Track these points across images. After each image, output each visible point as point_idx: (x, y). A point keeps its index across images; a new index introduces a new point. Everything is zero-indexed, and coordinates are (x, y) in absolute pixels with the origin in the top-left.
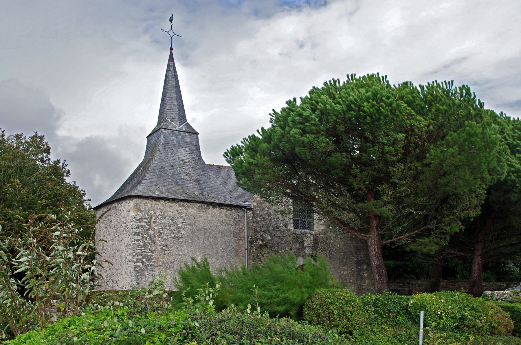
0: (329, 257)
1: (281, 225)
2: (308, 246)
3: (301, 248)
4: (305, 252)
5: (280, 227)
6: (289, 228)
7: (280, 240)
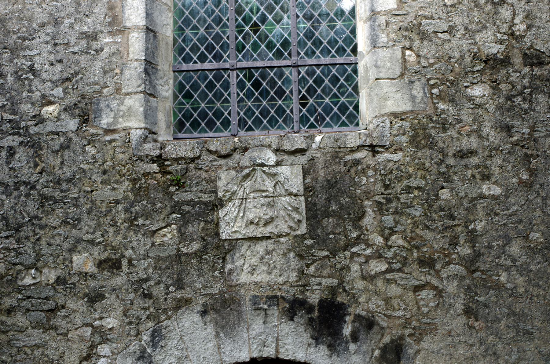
0: (468, 312)
1: (51, 110)
2: (251, 231)
3: (199, 255)
4: (226, 276)
5: (39, 120)
6: (105, 121)
7: (32, 207)
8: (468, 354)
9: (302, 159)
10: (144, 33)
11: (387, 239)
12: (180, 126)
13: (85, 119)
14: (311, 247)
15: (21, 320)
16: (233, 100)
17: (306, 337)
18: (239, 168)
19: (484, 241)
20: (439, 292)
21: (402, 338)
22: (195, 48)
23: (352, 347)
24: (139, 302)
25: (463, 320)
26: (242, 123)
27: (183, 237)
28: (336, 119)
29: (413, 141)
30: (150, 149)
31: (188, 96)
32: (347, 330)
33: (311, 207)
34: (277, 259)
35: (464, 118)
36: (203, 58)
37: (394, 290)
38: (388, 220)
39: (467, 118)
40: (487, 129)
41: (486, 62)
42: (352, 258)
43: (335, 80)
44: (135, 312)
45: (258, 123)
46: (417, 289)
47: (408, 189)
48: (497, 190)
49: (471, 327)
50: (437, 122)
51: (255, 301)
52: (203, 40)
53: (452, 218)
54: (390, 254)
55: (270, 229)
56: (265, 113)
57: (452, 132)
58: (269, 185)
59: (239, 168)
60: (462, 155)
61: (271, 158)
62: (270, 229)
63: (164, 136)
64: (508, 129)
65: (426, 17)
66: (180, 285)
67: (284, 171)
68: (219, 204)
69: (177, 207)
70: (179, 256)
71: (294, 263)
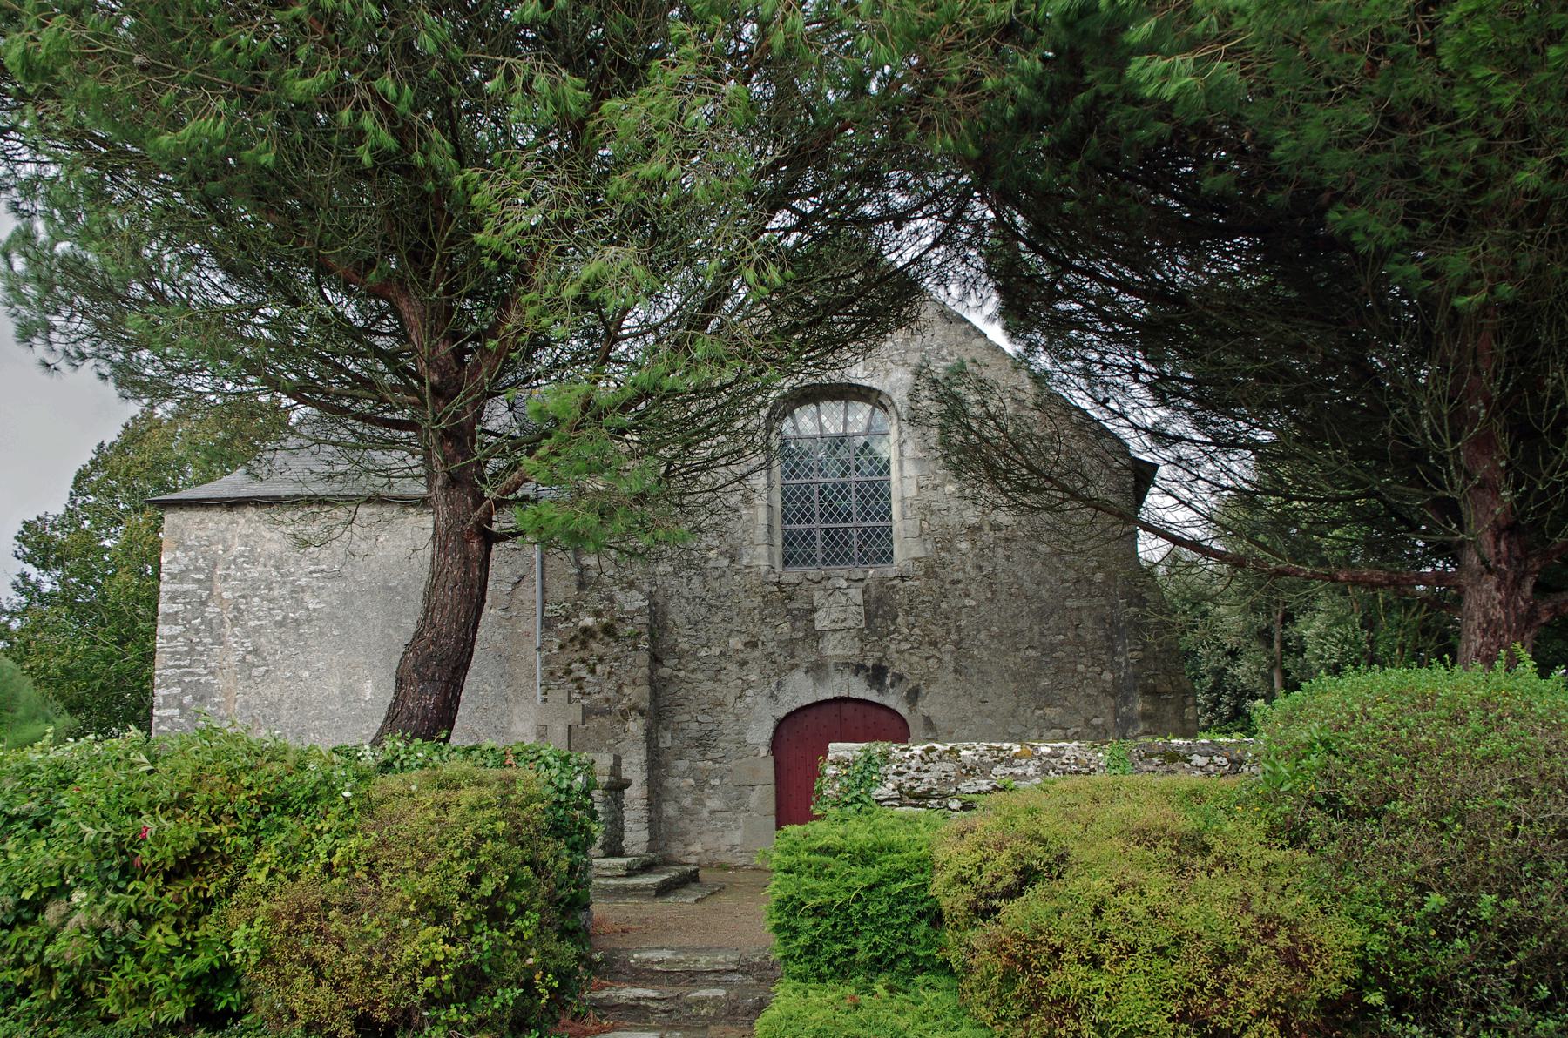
0: (956, 671)
1: (713, 554)
2: (834, 626)
3: (803, 639)
5: (707, 560)
6: (745, 561)
7: (704, 611)
9: (862, 585)
10: (822, 406)
12: (786, 563)
13: (733, 560)
15: (700, 676)
16: (818, 547)
17: (865, 685)
18: (825, 589)
20: (940, 660)
22: (794, 516)
24: (769, 666)
26: (824, 561)
27: (794, 629)
28: (879, 559)
29: (926, 574)
30: (773, 578)
31: (791, 544)
32: (888, 681)
33: (867, 612)
34: (848, 641)
36: (799, 522)
37: (915, 659)
38: (911, 620)
39: (957, 561)
40: (968, 568)
43: (879, 536)
44: (767, 671)
45: (833, 561)
46: (928, 658)
47: (923, 602)
48: (973, 603)
51: (836, 665)
52: (799, 510)
56: (837, 555)
58: (843, 599)
59: (825, 589)
60: (954, 582)
61: (844, 584)
63: (778, 569)
64: (980, 568)
66: (792, 656)
67: (852, 592)
68: (814, 610)
69: (789, 612)
70: (791, 640)
71: (858, 644)
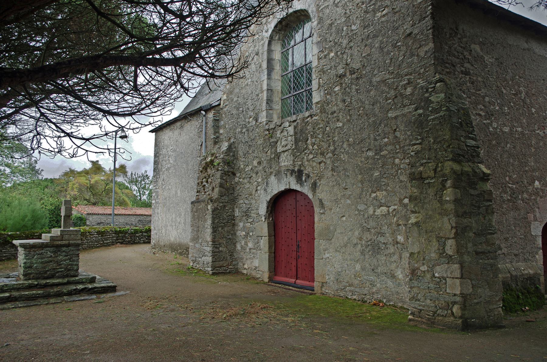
0: (333, 170)
8: (332, 185)
11: (313, 147)
14: (295, 152)
19: (337, 144)
21: (316, 180)
23: (305, 184)
25: (331, 173)
29: (321, 112)
33: (296, 139)
35: (333, 100)
41: (340, 77)
42: (305, 154)
49: (333, 175)
50: (326, 103)
53: (329, 137)
54: (313, 152)
55: (287, 148)
57: (330, 106)
62: (287, 148)
65: (325, 65)
